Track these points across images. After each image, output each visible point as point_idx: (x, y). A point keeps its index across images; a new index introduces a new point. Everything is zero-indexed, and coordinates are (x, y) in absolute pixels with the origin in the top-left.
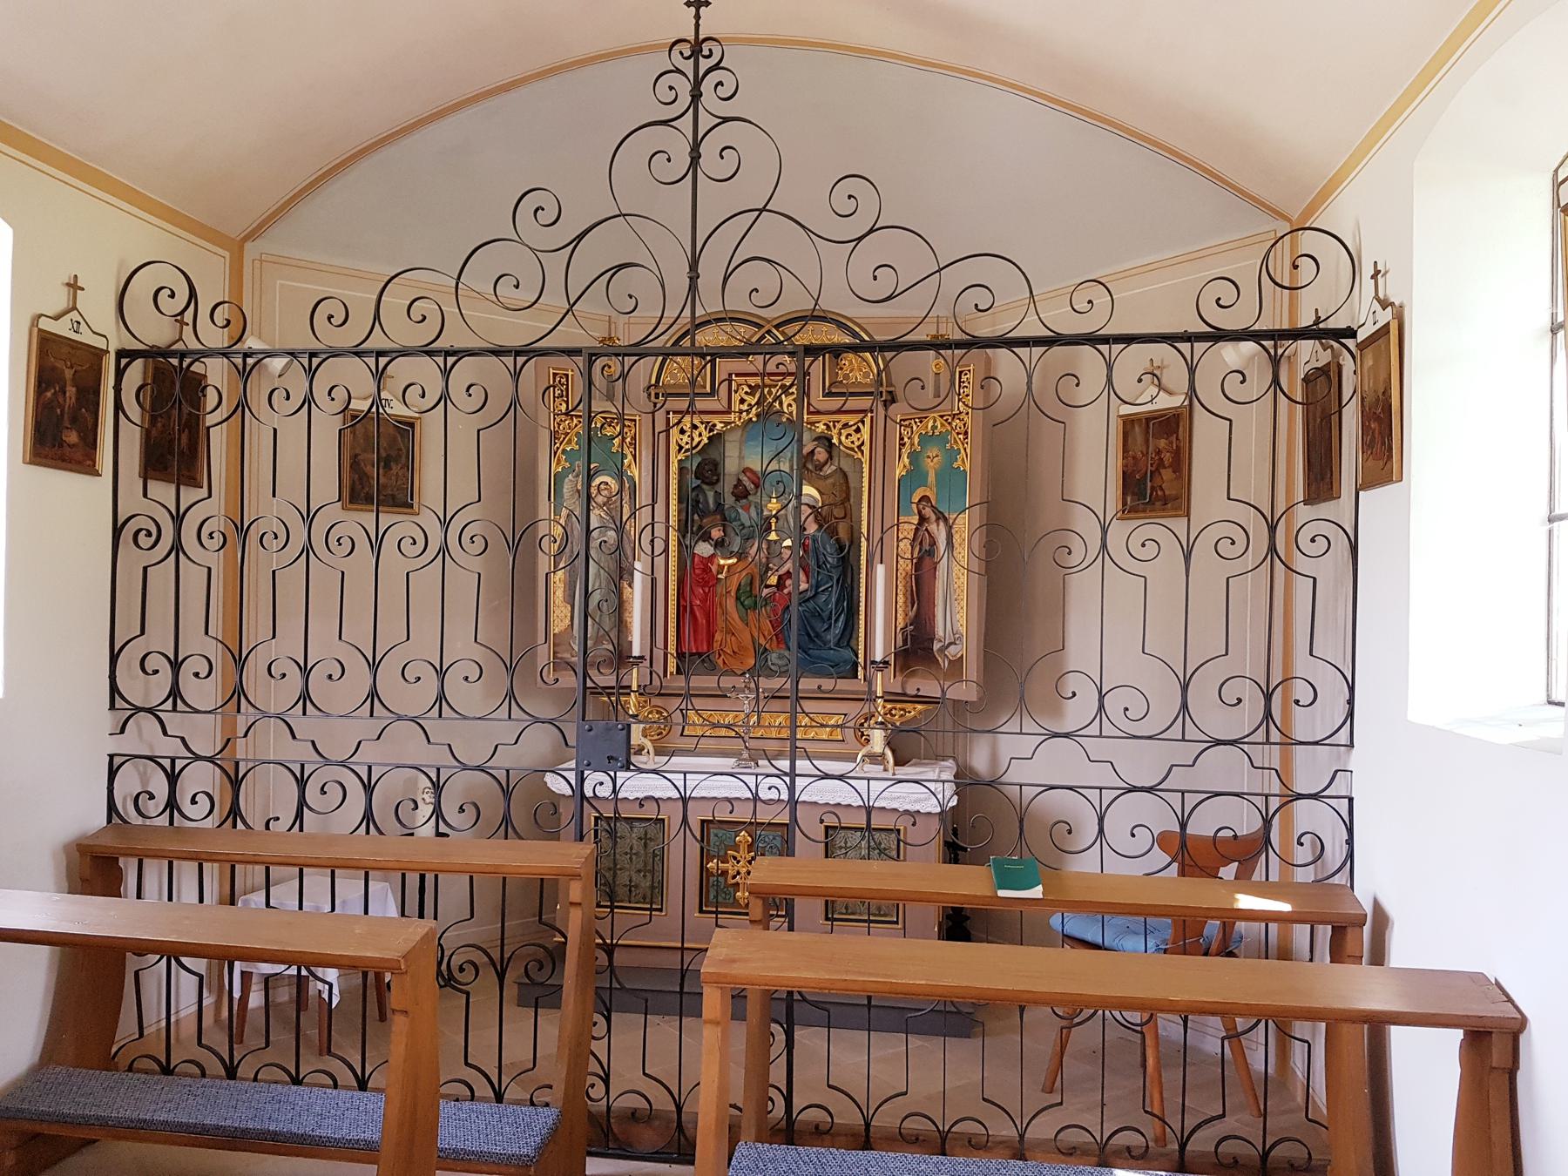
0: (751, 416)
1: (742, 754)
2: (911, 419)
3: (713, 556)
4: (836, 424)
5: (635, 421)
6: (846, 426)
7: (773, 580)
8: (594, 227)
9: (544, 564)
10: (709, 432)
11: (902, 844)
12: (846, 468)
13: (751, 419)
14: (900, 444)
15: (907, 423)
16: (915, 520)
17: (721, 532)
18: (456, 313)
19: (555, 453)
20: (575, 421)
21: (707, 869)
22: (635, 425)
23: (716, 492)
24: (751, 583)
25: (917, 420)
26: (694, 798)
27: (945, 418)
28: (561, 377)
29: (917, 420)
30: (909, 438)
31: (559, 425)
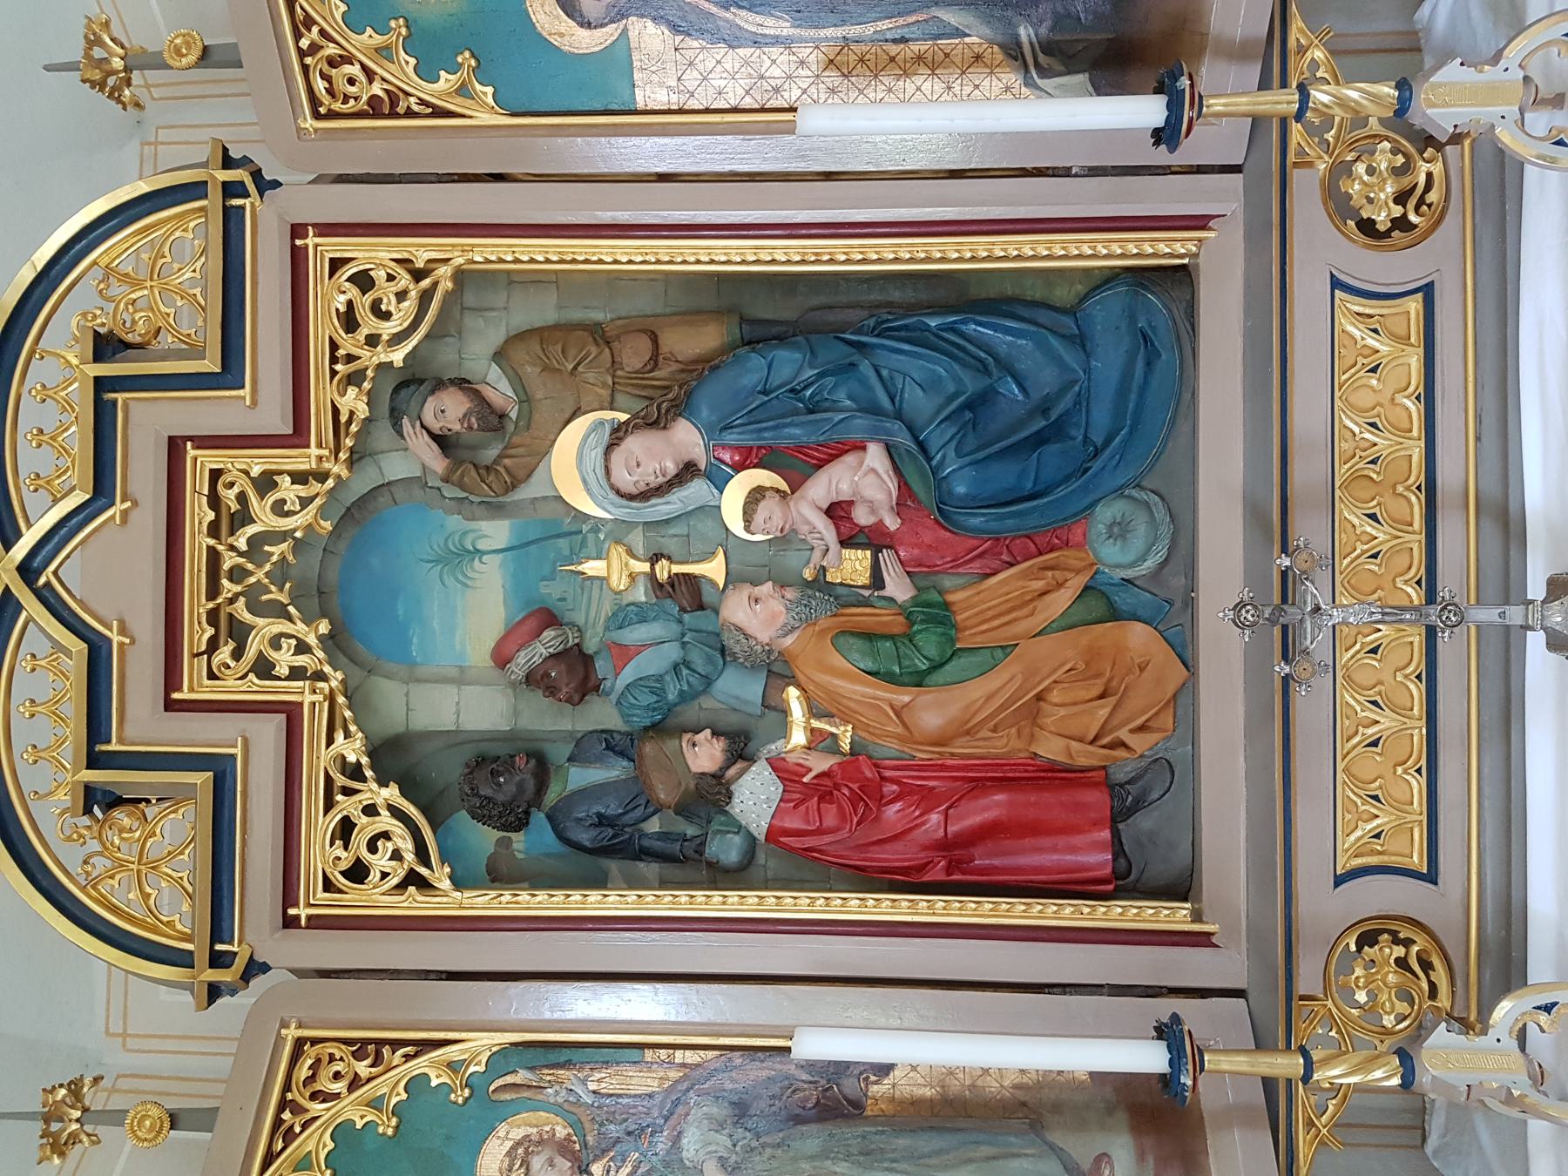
3: (778, 765)
5: (299, 1043)
6: (349, 321)
7: (854, 566)
10: (364, 779)
13: (321, 638)
14: (393, 115)
15: (320, 85)
23: (569, 760)
24: (869, 636)
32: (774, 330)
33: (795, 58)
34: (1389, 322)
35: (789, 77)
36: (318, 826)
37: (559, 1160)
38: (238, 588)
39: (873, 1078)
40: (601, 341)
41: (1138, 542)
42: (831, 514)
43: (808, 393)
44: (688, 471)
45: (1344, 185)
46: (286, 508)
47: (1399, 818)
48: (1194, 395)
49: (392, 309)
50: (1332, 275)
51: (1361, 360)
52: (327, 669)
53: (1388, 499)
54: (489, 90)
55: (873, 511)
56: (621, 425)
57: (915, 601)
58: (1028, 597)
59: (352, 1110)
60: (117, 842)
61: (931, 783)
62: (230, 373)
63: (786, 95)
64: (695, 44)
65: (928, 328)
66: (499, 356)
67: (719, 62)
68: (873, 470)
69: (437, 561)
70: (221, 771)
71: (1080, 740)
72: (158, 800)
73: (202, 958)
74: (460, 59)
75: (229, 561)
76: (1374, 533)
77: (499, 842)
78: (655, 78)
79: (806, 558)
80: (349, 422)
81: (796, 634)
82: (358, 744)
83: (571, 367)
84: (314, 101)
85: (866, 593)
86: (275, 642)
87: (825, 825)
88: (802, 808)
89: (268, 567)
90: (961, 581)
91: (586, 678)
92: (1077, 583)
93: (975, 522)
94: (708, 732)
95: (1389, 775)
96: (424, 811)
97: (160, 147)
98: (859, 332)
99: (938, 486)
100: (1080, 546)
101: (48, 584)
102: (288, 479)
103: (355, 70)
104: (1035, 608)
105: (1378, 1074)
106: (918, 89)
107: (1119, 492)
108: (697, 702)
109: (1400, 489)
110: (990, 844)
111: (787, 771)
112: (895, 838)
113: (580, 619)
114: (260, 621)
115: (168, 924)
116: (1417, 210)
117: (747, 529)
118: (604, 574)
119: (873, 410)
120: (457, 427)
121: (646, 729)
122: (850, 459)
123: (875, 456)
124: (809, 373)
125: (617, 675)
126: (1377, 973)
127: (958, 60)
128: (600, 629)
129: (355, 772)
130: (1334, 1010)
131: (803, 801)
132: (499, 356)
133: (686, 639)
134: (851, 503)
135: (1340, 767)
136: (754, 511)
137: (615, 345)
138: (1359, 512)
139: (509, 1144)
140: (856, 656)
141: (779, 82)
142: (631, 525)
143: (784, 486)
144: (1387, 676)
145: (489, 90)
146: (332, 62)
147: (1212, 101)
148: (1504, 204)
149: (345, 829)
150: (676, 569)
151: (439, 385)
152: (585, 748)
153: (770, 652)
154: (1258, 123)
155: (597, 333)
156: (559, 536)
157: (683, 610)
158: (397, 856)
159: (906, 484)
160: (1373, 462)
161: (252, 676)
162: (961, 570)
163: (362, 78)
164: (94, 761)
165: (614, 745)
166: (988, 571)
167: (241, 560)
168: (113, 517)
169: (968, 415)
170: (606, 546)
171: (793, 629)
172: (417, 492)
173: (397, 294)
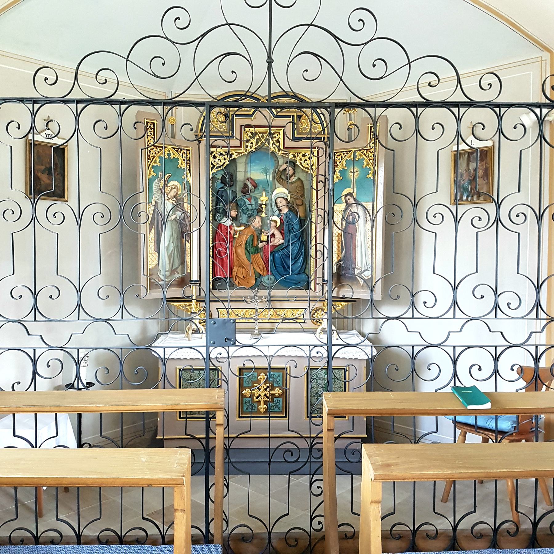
1: (254, 331)
2: (341, 152)
4: (299, 154)
5: (189, 150)
6: (304, 155)
7: (264, 238)
8: (213, 30)
9: (143, 229)
10: (230, 158)
11: (288, 376)
12: (302, 179)
15: (339, 154)
16: (343, 206)
17: (236, 213)
18: (80, 83)
19: (148, 167)
21: (242, 394)
22: (190, 153)
23: (232, 191)
24: (253, 240)
25: (344, 152)
26: (170, 359)
27: (362, 151)
28: (150, 124)
29: (344, 152)
30: (340, 162)
31: (150, 152)
36: (222, 151)
37: (175, 193)
38: (261, 137)
42: (62, 194)
45: (320, 310)
52: (247, 152)
54: (337, 181)
55: (273, 241)
56: (287, 200)
57: (258, 248)
59: (180, 161)
65: (302, 249)
66: (299, 179)
68: (279, 241)
75: (265, 135)
77: (218, 179)
84: (337, 153)
86: (252, 143)
92: (261, 273)
94: (237, 214)
98: (302, 238)
99: (277, 251)
103: (340, 160)
113: (256, 192)
114: (255, 140)
116: (316, 321)
118: (263, 196)
121: (237, 203)
122: (281, 237)
123: (282, 241)
125: (246, 198)
128: (254, 195)
129: (231, 156)
132: (299, 179)
134: (274, 237)
139: (177, 185)
143: (277, 226)
145: (337, 181)
146: (342, 156)
150: (264, 208)
151: (294, 169)
155: (303, 195)
157: (257, 209)
167: (265, 137)
172: (277, 165)
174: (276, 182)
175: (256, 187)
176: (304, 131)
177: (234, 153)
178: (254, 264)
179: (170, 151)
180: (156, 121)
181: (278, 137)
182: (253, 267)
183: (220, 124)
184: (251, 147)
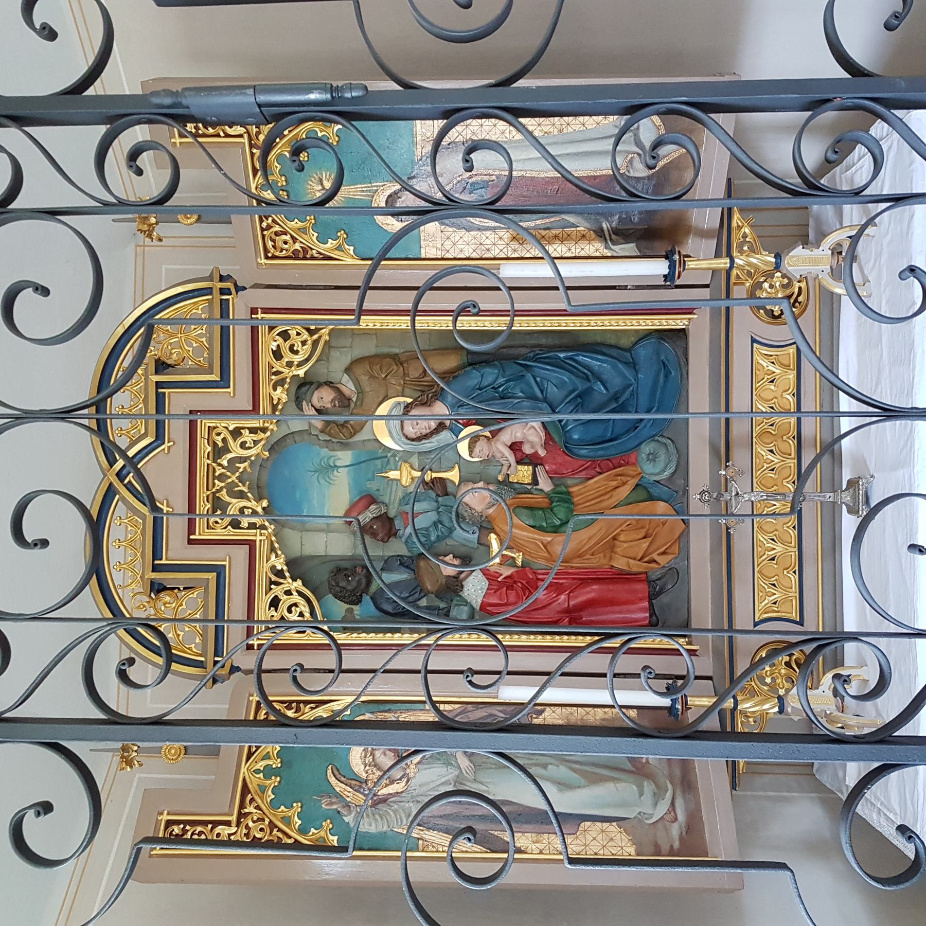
0: (259, 510)
3: (485, 572)
7: (523, 474)
10: (285, 578)
12: (346, 361)
13: (264, 509)
14: (305, 258)
15: (270, 244)
20: (250, 809)
23: (382, 570)
24: (531, 508)
25: (264, 225)
29: (264, 225)
30: (294, 240)
32: (483, 358)
33: (496, 236)
34: (780, 358)
35: (494, 244)
38: (223, 484)
39: (534, 716)
40: (399, 364)
41: (661, 464)
43: (501, 389)
44: (441, 427)
46: (247, 446)
47: (785, 594)
48: (687, 392)
49: (299, 349)
50: (752, 337)
51: (766, 377)
53: (780, 443)
54: (352, 248)
55: (533, 447)
57: (554, 491)
58: (609, 490)
60: (163, 608)
61: (561, 581)
62: (224, 381)
63: (492, 252)
64: (451, 229)
66: (348, 370)
67: (461, 237)
69: (316, 471)
70: (219, 571)
71: (634, 559)
72: (185, 588)
73: (210, 664)
74: (339, 234)
76: (773, 459)
77: (347, 610)
78: (431, 244)
79: (498, 470)
80: (278, 403)
81: (495, 507)
82: (282, 560)
83: (384, 376)
84: (266, 250)
85: (529, 487)
87: (510, 600)
88: (498, 592)
89: (237, 474)
90: (576, 481)
91: (390, 530)
92: (633, 482)
93: (583, 452)
94: (451, 555)
95: (781, 575)
96: (313, 593)
97: (146, 248)
99: (565, 435)
100: (634, 464)
101: (130, 482)
102: (248, 431)
103: (287, 238)
104: (612, 495)
105: (766, 706)
106: (555, 250)
107: (652, 438)
108: (445, 541)
109: (785, 438)
110: (590, 610)
111: (490, 575)
112: (544, 607)
114: (234, 501)
115: (189, 649)
117: (471, 455)
119: (533, 398)
120: (329, 406)
124: (501, 380)
125: (405, 528)
126: (776, 669)
127: (574, 237)
128: (396, 505)
129: (280, 574)
130: (755, 686)
131: (498, 590)
132: (348, 370)
133: (440, 510)
134: (521, 443)
135: (756, 570)
136: (475, 447)
137: (405, 365)
138: (765, 449)
140: (524, 518)
141: (489, 246)
142: (412, 454)
144: (779, 527)
145: (352, 248)
146: (277, 234)
147: (689, 263)
148: (832, 304)
149: (275, 603)
150: (434, 475)
151: (320, 385)
152: (388, 564)
153: (481, 516)
154: (715, 272)
156: (377, 459)
157: (438, 495)
158: (301, 614)
159: (549, 434)
160: (772, 425)
161: (229, 527)
162: (576, 476)
163: (291, 241)
164: (155, 569)
165: (405, 563)
166: (589, 476)
167: (224, 471)
168: (164, 449)
169: (579, 400)
170: (400, 463)
171: (494, 505)
172: (306, 437)
173: (301, 342)
174: (357, 438)
175: (370, 500)
176: (205, 355)
177: (270, 564)
178: (604, 504)
179: (257, 767)
180: (162, 814)
181: (225, 433)
182: (615, 507)
183: (184, 607)
184: (255, 513)
